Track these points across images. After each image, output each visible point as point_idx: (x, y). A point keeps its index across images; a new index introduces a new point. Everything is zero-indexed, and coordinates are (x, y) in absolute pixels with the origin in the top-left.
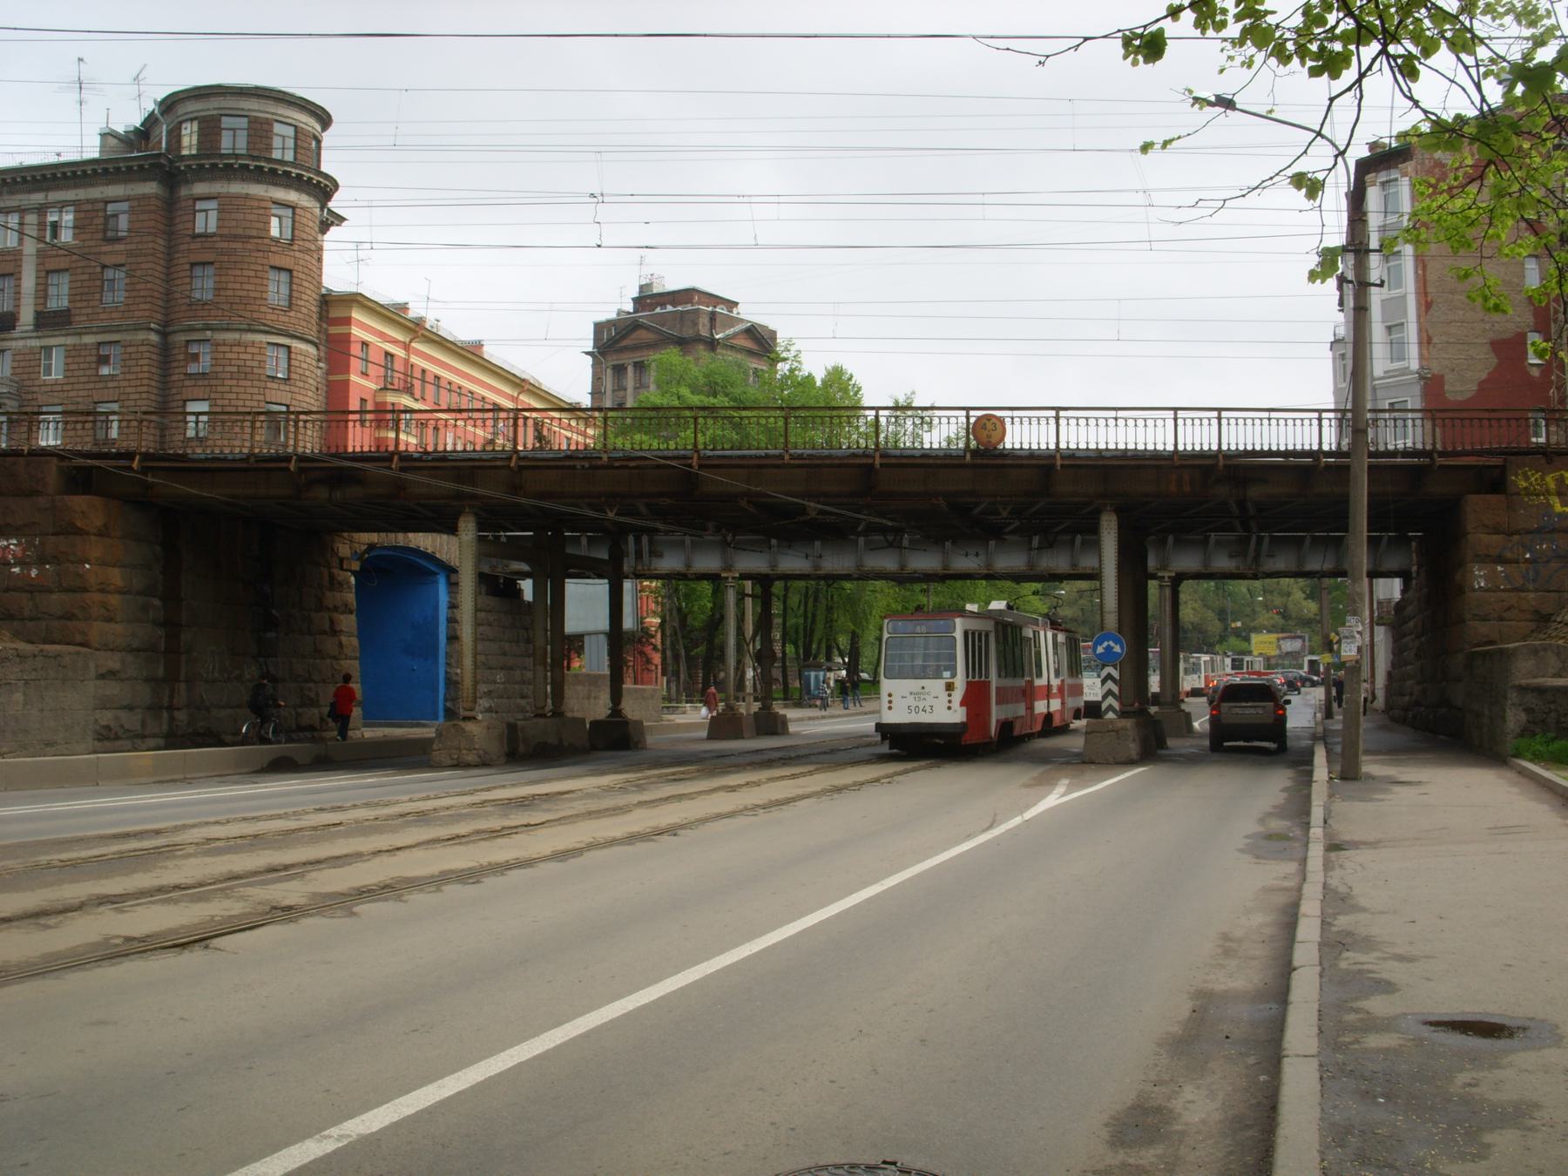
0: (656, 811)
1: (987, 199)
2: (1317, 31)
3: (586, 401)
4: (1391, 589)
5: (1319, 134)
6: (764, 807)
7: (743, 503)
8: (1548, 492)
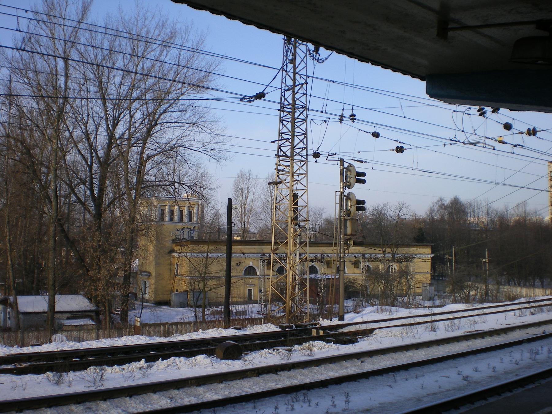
0: (305, 371)
1: (456, 315)
2: (149, 406)
3: (57, 309)
4: (321, 319)
5: (87, 99)
6: (499, 141)
7: (49, 211)
8: (207, 258)
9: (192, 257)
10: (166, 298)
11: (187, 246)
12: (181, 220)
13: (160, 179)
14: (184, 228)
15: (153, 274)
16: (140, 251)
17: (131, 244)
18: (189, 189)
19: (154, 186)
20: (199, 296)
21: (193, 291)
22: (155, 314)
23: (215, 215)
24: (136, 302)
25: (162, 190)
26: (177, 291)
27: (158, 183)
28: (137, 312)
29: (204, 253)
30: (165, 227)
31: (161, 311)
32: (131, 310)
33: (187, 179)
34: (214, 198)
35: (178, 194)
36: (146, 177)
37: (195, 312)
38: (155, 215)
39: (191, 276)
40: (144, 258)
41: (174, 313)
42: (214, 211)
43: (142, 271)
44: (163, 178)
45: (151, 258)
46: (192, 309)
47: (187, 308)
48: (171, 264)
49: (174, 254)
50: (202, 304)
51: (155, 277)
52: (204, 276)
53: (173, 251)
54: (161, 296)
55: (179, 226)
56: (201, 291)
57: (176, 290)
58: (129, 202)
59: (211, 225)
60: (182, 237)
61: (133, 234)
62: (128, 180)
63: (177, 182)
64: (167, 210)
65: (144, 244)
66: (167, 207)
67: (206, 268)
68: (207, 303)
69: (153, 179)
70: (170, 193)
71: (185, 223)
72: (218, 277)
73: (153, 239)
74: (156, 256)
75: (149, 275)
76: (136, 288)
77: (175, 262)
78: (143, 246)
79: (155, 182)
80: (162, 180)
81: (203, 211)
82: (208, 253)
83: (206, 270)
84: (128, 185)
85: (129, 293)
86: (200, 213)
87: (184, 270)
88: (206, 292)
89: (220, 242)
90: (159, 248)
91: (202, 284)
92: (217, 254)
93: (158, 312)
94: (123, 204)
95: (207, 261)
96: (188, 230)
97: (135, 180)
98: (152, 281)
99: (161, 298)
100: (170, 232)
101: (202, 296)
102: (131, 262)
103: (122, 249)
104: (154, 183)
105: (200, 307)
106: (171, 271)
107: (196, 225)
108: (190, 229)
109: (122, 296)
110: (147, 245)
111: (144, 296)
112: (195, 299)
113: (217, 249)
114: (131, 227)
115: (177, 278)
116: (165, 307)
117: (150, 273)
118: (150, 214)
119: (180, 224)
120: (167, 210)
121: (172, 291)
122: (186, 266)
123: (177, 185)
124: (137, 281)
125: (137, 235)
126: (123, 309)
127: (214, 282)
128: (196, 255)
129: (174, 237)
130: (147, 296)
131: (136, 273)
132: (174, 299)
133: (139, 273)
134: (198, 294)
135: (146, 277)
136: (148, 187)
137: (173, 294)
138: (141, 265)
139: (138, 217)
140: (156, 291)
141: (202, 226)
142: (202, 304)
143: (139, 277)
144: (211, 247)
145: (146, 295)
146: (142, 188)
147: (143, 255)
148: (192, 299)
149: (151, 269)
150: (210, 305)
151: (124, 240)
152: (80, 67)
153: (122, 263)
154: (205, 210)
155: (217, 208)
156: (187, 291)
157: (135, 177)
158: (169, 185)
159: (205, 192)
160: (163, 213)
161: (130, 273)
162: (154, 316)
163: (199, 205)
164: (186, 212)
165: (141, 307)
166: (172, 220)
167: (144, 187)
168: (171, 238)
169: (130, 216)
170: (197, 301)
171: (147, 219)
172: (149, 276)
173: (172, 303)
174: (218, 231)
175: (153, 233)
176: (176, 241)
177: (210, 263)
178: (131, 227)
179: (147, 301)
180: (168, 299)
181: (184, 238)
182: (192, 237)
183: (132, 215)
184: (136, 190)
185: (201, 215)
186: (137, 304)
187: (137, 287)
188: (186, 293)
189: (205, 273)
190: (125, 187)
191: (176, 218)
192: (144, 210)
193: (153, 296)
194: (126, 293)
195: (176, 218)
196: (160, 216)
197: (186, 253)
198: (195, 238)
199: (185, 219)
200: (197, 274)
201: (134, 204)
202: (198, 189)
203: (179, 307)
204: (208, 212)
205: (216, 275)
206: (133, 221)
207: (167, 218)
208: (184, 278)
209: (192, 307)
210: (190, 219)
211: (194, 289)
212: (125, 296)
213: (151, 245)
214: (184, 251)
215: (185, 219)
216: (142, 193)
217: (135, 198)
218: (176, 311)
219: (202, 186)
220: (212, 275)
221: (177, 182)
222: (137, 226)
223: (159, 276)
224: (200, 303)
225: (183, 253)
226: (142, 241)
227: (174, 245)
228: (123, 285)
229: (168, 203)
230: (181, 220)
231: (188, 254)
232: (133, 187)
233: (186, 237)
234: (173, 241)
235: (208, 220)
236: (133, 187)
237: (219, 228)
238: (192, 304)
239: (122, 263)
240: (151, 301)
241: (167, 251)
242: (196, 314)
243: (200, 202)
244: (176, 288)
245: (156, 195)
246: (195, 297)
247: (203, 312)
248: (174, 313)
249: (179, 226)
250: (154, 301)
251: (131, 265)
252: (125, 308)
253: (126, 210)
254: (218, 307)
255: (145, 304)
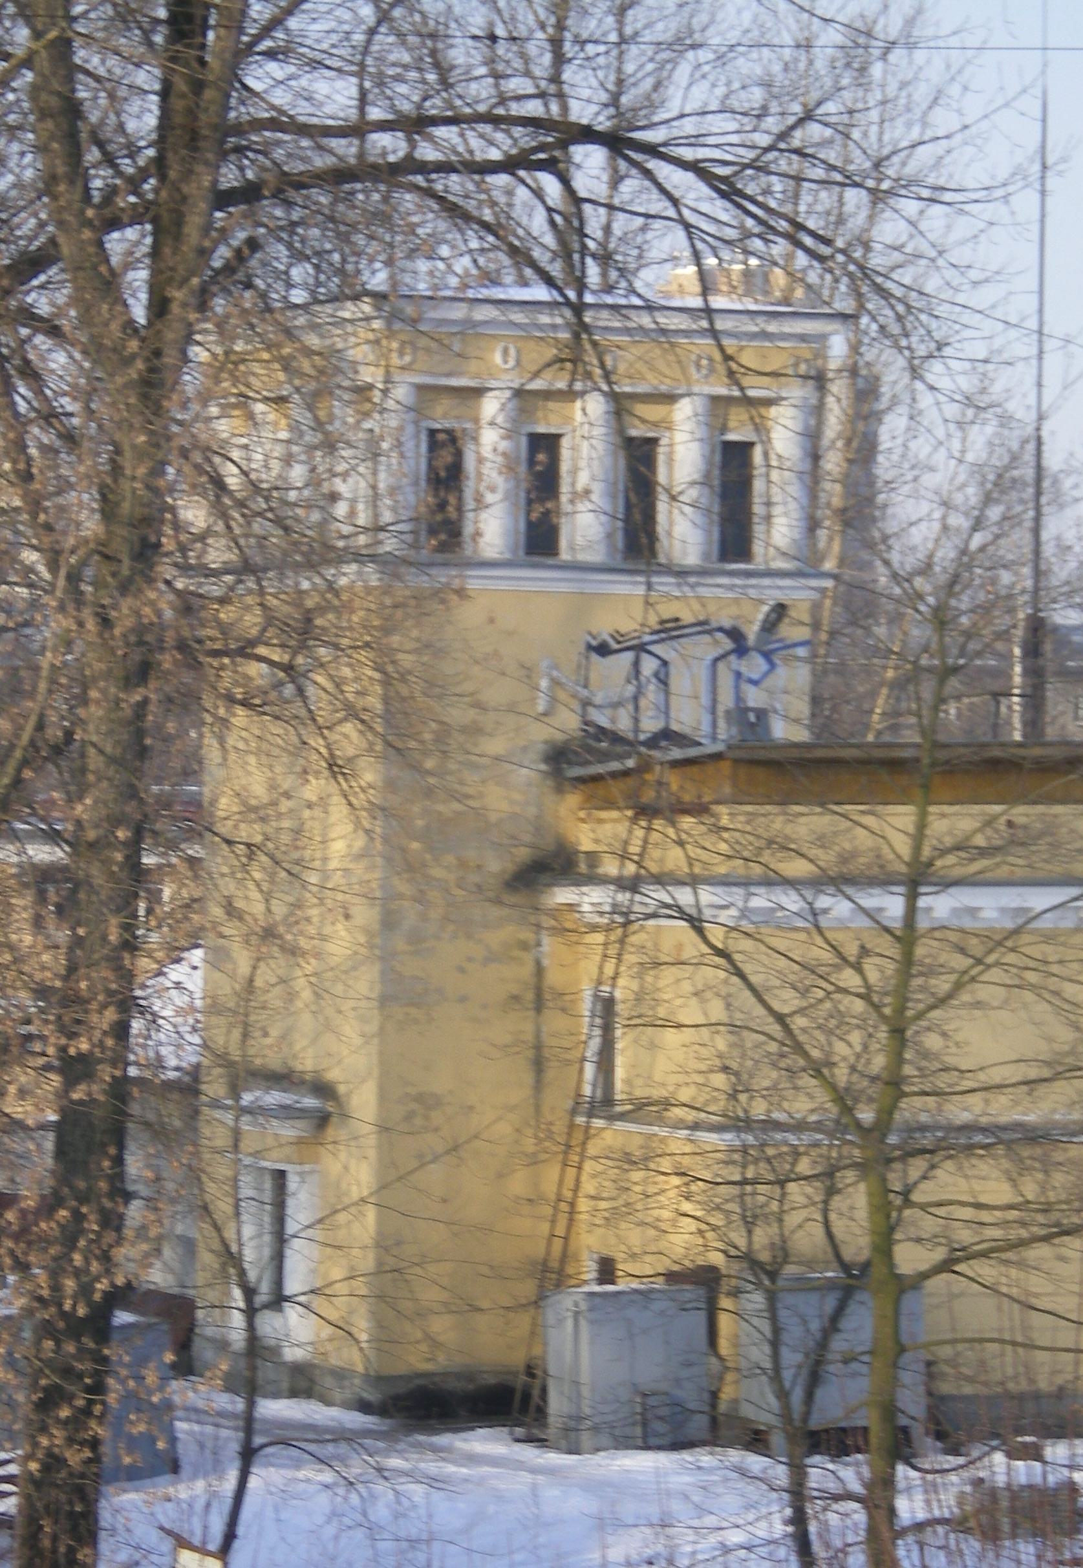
8: (907, 935)
9: (752, 928)
10: (485, 1345)
11: (699, 810)
12: (637, 540)
13: (406, 96)
14: (670, 630)
15: (363, 1102)
16: (220, 863)
17: (132, 793)
18: (721, 209)
19: (355, 182)
20: (833, 1324)
21: (766, 1271)
22: (381, 1512)
23: (998, 486)
24: (181, 1391)
25: (430, 223)
26: (607, 1270)
27: (389, 145)
28: (190, 1490)
29: (883, 880)
30: (469, 615)
31: (434, 1482)
32: (133, 1475)
33: (699, 96)
34: (983, 297)
35: (605, 258)
36: (261, 76)
37: (798, 1494)
38: (367, 492)
39: (743, 1124)
40: (269, 934)
41: (577, 1504)
42: (980, 436)
43: (243, 1075)
44: (445, 83)
45: (342, 941)
46: (756, 1462)
47: (705, 1458)
48: (540, 997)
49: (563, 895)
50: (869, 1418)
51: (384, 1128)
52: (883, 1125)
53: (554, 864)
54: (441, 1326)
55: (624, 605)
56: (853, 1280)
57: (589, 1269)
58: (95, 350)
59: (953, 585)
60: (650, 725)
61: (151, 691)
62: (73, 110)
63: (587, 134)
64: (491, 443)
65: (259, 790)
66: (491, 407)
67: (898, 1033)
68: (912, 1402)
69: (335, 97)
70: (520, 256)
71: (682, 573)
72: (1033, 1136)
73: (349, 738)
74: (389, 922)
75: (320, 1108)
76: (189, 1246)
77: (581, 971)
78: (252, 811)
79: (359, 129)
80: (434, 107)
81: (863, 450)
82: (917, 879)
83: (898, 1060)
84: (78, 173)
85: (121, 1296)
86: (833, 462)
87: (673, 1058)
88: (904, 1286)
89: (1046, 768)
90: (408, 840)
91: (855, 1203)
92: (1012, 898)
93: (417, 1491)
94: (31, 374)
95: (907, 961)
96: (705, 649)
97: (143, 119)
98: (353, 1165)
99: (445, 1344)
100: (528, 672)
101: (861, 1324)
102: (128, 977)
103: (43, 853)
104: (346, 148)
105: (838, 1442)
106: (539, 1064)
107: (799, 595)
108: (735, 634)
109: (46, 1330)
110: (291, 798)
111: (269, 1324)
112: (791, 1358)
113: (1018, 839)
114: (124, 614)
115: (611, 1135)
116: (486, 1442)
117: (323, 1089)
118: (314, 481)
119: (630, 588)
120: (491, 443)
121: (551, 1275)
122: (691, 1013)
123: (590, 164)
124: (195, 1175)
125: (185, 703)
126: (53, 1462)
127: (990, 1182)
128: (791, 901)
129: (568, 722)
130: (296, 1332)
131: (189, 1087)
132: (579, 1356)
133: (214, 1087)
134: (812, 1310)
135: (288, 1131)
136: (287, 185)
137: (567, 1301)
138: (239, 1007)
139: (195, 513)
140: (391, 1277)
141: (857, 603)
142: (869, 1418)
143: (216, 1128)
144: (954, 821)
145: (293, 1314)
146: (223, 199)
147: (253, 904)
148: (761, 1355)
149: (343, 1045)
150: (953, 1427)
151: (57, 751)
152: (354, 334)
153: (41, 992)
154: (891, 430)
155: (1021, 408)
156: (706, 1279)
157: (147, 77)
158: (509, 165)
159: (889, 229)
160: (445, 470)
161: (120, 1089)
162: (373, 1530)
163: (820, 380)
164: (684, 458)
165: (232, 1439)
166: (540, 540)
167: (249, 193)
168: (541, 734)
169: (108, 509)
170: (815, 1379)
171: (288, 539)
172: (322, 1120)
173: (557, 1405)
174: (1032, 650)
175: (358, 676)
176: (586, 762)
177: (942, 985)
178: (124, 614)
179: (303, 1381)
180: (517, 1358)
181: (667, 735)
182: (754, 722)
183: (132, 487)
184: (166, 225)
185: (846, 480)
186: (196, 1414)
187: (200, 1231)
188: (691, 1293)
189: (894, 1085)
190: (48, 184)
191: (586, 526)
192: (257, 444)
193: (363, 1328)
194: (85, 1291)
195: (586, 526)
196: (415, 498)
197: (693, 881)
198: (780, 730)
199: (683, 531)
200: (807, 1102)
201: (148, 375)
202: (814, 207)
203: (624, 1443)
204: (921, 447)
205: (1003, 1110)
206: (146, 551)
207: (493, 526)
208: (678, 1142)
209: (756, 1441)
210: (734, 536)
211: (783, 1251)
212: (75, 1328)
213: (338, 810)
214: (675, 859)
215: (683, 531)
216: (221, 256)
217: (159, 306)
218: (593, 1486)
219: (860, 163)
220: (960, 1112)
221: (587, 134)
222: (188, 605)
223: (412, 1111)
224: (844, 1398)
225: (660, 880)
226: (239, 766)
227: (573, 799)
228: (49, 1206)
229: (501, 367)
230: (637, 540)
231: (707, 895)
232: (134, 184)
233: (688, 716)
234: (558, 757)
235: (922, 536)
236: (134, 184)
237: (1037, 627)
238: (758, 1402)
239: (41, 992)
240: (341, 1375)
241: (497, 865)
242: (799, 1520)
243: (838, 346)
244: (591, 1242)
245: (378, 280)
246: (793, 1333)
247: (879, 1498)
248: (577, 1504)
249: (624, 605)
250: (378, 1380)
251: (127, 1005)
252: (75, 1457)
253: (70, 438)
254: (1034, 1454)
255: (272, 1408)
